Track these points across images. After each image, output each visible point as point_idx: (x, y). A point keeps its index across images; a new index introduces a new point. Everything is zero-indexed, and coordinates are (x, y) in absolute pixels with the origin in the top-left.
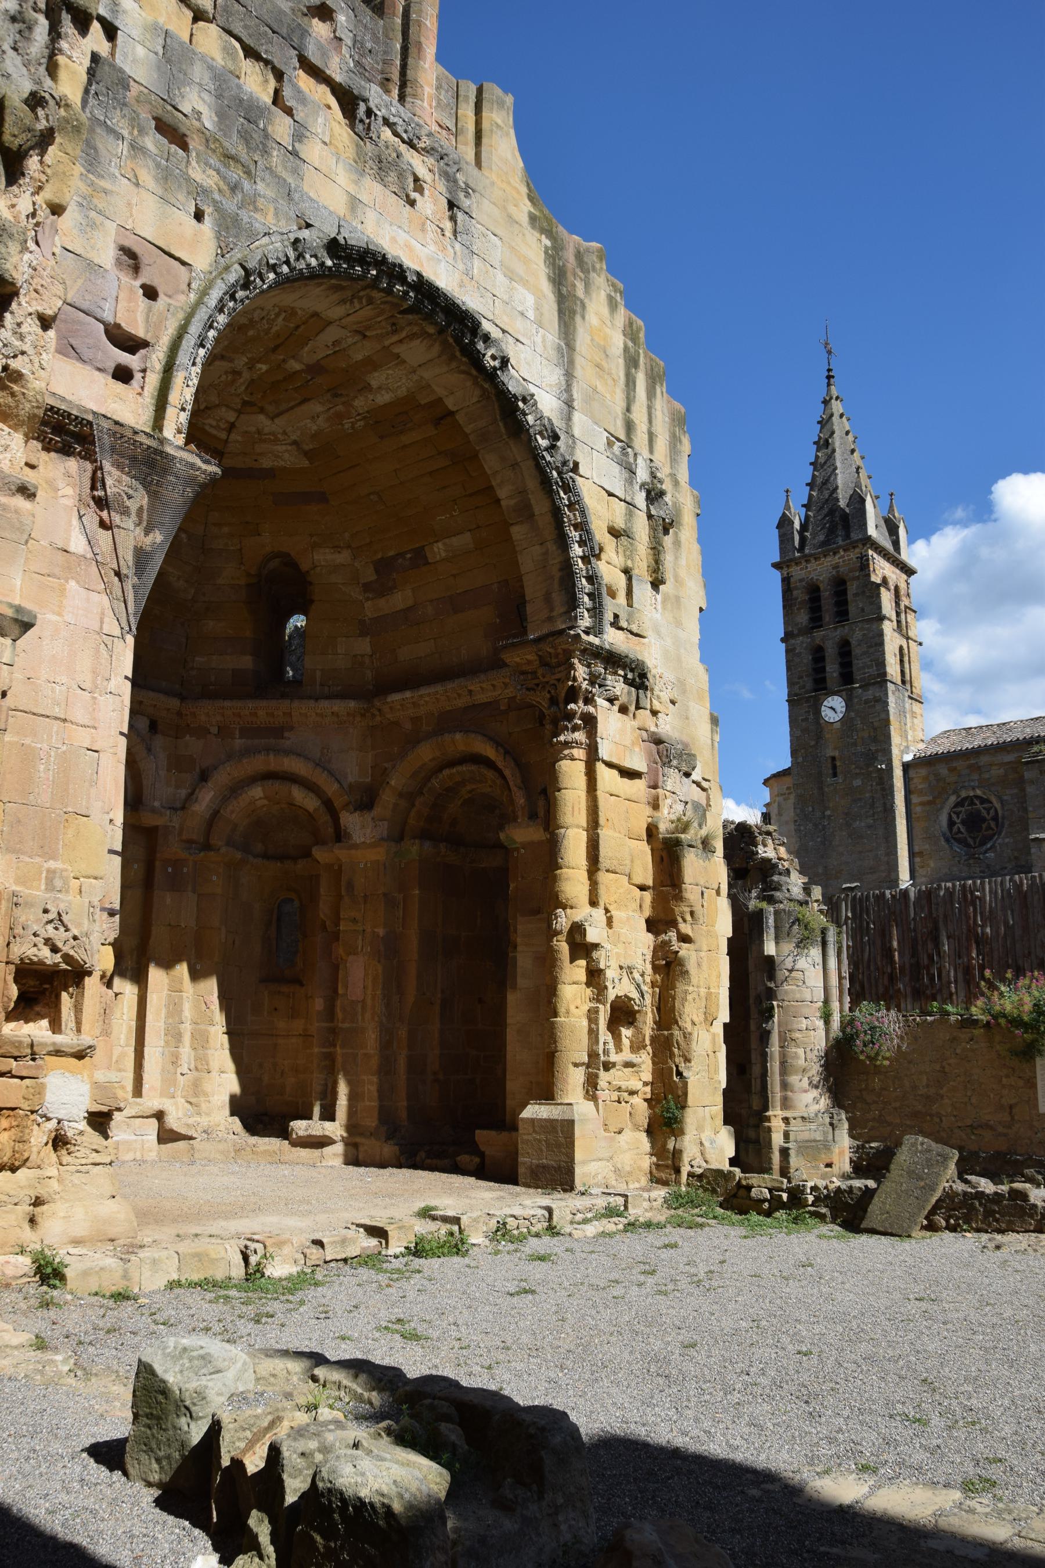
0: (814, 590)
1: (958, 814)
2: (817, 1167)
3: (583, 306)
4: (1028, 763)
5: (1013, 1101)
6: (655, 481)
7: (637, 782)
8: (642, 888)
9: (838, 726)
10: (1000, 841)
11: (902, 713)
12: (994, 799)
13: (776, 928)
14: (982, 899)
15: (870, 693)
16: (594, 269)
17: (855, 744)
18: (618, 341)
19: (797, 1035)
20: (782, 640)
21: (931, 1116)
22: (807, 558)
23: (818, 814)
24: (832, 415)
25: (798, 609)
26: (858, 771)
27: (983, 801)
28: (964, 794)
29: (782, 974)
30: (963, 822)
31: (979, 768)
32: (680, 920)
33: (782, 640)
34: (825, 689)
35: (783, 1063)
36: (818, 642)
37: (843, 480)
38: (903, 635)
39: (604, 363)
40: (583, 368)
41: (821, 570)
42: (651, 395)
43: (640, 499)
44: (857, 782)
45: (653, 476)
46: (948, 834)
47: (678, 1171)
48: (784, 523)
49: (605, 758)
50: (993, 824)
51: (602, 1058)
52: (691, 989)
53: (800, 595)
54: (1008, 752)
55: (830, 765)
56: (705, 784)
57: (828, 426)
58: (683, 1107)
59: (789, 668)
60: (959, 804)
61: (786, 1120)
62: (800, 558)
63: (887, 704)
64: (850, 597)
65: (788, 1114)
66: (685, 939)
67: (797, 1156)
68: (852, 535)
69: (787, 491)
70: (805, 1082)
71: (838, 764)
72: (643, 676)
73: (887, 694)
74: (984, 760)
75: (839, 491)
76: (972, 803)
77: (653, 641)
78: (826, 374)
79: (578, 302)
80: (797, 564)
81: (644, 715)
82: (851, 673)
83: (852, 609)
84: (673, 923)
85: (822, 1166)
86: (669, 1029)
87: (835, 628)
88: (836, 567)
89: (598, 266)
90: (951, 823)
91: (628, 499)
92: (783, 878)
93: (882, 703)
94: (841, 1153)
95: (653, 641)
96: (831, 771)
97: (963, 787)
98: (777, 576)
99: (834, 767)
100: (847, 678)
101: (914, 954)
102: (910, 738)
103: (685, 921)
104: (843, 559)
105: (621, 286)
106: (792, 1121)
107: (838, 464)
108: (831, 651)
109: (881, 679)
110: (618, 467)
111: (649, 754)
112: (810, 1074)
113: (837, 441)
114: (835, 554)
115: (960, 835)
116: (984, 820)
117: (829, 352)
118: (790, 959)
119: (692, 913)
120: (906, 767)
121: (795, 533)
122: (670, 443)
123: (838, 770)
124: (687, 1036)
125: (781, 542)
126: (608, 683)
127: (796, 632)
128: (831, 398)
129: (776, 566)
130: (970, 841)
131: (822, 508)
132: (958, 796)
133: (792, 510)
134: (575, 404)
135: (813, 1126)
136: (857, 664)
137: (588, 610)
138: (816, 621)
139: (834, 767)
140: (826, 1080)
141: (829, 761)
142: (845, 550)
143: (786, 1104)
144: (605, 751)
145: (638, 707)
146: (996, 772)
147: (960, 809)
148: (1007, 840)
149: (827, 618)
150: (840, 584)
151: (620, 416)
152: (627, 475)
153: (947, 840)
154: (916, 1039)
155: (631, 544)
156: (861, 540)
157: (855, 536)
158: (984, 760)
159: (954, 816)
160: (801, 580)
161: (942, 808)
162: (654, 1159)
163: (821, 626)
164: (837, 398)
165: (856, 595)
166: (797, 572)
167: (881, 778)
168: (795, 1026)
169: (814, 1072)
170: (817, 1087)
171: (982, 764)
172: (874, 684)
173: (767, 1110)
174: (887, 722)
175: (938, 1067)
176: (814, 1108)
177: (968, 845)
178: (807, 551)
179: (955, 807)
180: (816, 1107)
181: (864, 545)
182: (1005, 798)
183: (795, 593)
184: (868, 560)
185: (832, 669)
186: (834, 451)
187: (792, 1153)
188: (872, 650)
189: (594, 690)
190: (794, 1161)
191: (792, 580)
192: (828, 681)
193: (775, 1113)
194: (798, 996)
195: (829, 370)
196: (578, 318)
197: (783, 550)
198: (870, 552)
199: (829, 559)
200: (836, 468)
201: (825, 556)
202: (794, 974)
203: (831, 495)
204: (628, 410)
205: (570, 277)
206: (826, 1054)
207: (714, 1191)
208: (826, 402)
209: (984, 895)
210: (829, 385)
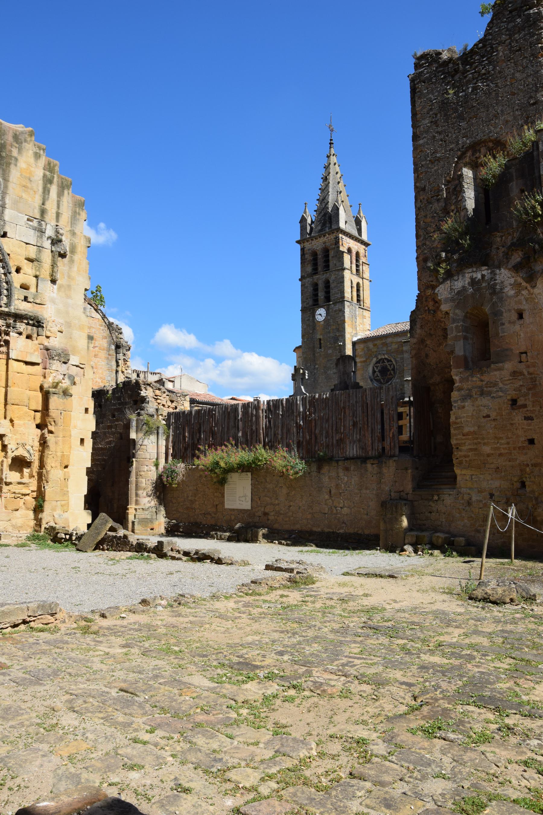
0: (314, 254)
1: (377, 367)
2: (147, 530)
3: (16, 159)
4: (405, 342)
5: (217, 503)
6: (58, 235)
7: (36, 367)
8: (36, 411)
9: (322, 323)
10: (394, 381)
11: (354, 317)
12: (393, 360)
13: (137, 427)
14: (215, 414)
15: (338, 307)
16: (26, 141)
17: (329, 332)
18: (39, 173)
19: (142, 473)
20: (300, 280)
21: (192, 509)
22: (312, 238)
23: (313, 367)
24: (330, 164)
25: (307, 264)
26: (330, 346)
27: (389, 361)
28: (380, 357)
29: (138, 446)
30: (379, 371)
31: (387, 344)
32: (49, 424)
33: (300, 280)
34: (318, 304)
35: (136, 485)
36: (315, 281)
37: (331, 198)
38: (360, 277)
39: (29, 185)
40: (13, 188)
41: (317, 245)
42: (60, 194)
43: (47, 244)
44: (330, 351)
45: (57, 232)
46: (372, 377)
47: (41, 527)
48: (303, 220)
49: (13, 358)
50: (392, 372)
51: (4, 480)
52: (50, 453)
53: (308, 257)
54: (400, 336)
55: (318, 343)
56: (81, 366)
57: (327, 170)
58: (44, 501)
59: (302, 294)
60: (378, 362)
61: (136, 509)
62: (309, 238)
63: (344, 312)
64: (330, 258)
65: (137, 507)
66: (51, 432)
67: (138, 524)
68: (333, 226)
69: (306, 204)
70: (145, 494)
71: (322, 342)
72: (39, 322)
73: (344, 307)
74: (389, 340)
75: (329, 204)
76: (384, 362)
77: (50, 306)
78: (330, 141)
79: (13, 159)
80: (307, 241)
81: (42, 339)
82: (329, 296)
83: (331, 264)
84: (46, 426)
85: (149, 529)
86: (42, 469)
87: (323, 274)
88: (325, 243)
89: (29, 139)
90: (374, 372)
91: (39, 245)
92: (146, 405)
93: (342, 311)
94: (160, 524)
95: (50, 306)
96: (319, 346)
97: (380, 354)
98: (298, 247)
99: (320, 344)
100: (328, 299)
101: (193, 439)
102: (358, 329)
103: (51, 425)
104: (328, 239)
105: (44, 146)
106: (138, 510)
107: (330, 190)
108: (321, 286)
109: (342, 300)
110: (33, 231)
111: (44, 355)
112: (147, 490)
113: (331, 178)
114: (324, 236)
115: (378, 378)
116: (389, 370)
117: (332, 130)
118: (141, 440)
119: (54, 421)
120: (354, 344)
121: (308, 225)
122: (72, 216)
123: (322, 345)
124: (47, 472)
125: (301, 230)
126: (17, 326)
127: (306, 276)
128: (330, 155)
129: (298, 242)
130: (382, 380)
131: (321, 212)
132: (377, 358)
133: (308, 213)
134: (7, 206)
135: (147, 512)
136: (332, 292)
137: (5, 296)
138: (315, 271)
139: (320, 344)
140: (155, 493)
141: (318, 340)
142: (329, 234)
143: (137, 503)
144: (12, 355)
145: (38, 335)
146: (394, 346)
147: (378, 365)
148: (397, 380)
149: (320, 269)
150: (326, 251)
151: (37, 207)
152: (39, 234)
153: (371, 380)
154: (189, 476)
155: (39, 265)
156: (336, 229)
157: (334, 227)
158: (389, 340)
159: (375, 368)
160: (309, 250)
161: (370, 364)
162: (35, 522)
163: (317, 273)
164: (334, 155)
165: (333, 257)
166: (307, 245)
167: (340, 349)
168: (142, 469)
169: (149, 489)
170: (150, 496)
171: (388, 342)
172: (339, 302)
173: (128, 505)
174: (344, 322)
175: (195, 488)
176: (148, 505)
177: (381, 383)
178: (312, 235)
179: (376, 363)
180: (149, 505)
181: (337, 232)
182: (398, 359)
183: (306, 256)
184: (339, 239)
185: (321, 295)
186: (329, 183)
187: (136, 523)
188: (339, 285)
189: (9, 330)
190: (136, 527)
191: (305, 249)
192: (319, 301)
193: (131, 506)
194: (143, 456)
195: (331, 140)
196: (12, 166)
197: (302, 234)
198: (340, 235)
199: (322, 239)
200: (329, 192)
201: (320, 237)
202: (142, 447)
203: (325, 206)
204: (43, 204)
205: (8, 147)
206: (156, 482)
207: (50, 535)
208: (328, 157)
209: (215, 413)
210: (330, 148)
